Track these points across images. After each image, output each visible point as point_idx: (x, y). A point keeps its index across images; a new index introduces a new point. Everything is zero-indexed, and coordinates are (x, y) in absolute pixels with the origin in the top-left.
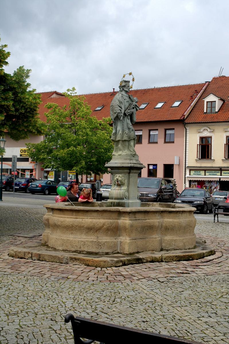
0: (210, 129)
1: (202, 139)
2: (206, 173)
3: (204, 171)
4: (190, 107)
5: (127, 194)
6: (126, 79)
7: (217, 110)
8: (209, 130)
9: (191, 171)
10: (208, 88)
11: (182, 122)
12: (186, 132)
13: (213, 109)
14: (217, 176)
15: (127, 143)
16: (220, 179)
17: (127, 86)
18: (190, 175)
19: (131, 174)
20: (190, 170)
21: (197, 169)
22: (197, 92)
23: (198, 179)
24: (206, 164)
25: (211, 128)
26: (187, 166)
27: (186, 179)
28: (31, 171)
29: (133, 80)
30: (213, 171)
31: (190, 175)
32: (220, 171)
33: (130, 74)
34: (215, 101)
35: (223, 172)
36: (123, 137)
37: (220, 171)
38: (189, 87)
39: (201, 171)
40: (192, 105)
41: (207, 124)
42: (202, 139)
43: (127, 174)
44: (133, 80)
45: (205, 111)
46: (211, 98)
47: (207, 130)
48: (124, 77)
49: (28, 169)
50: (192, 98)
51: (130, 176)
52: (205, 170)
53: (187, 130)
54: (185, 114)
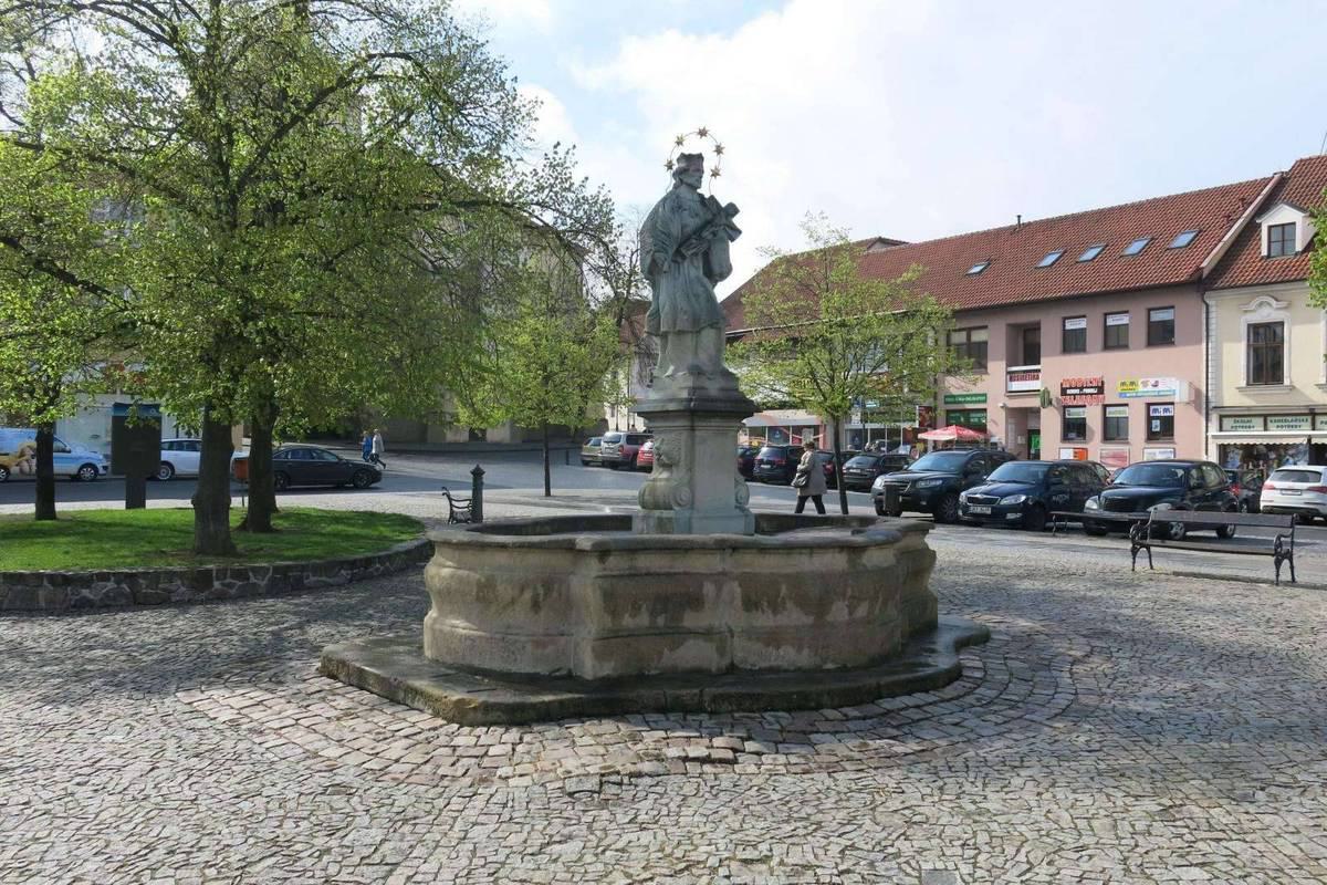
0: (1277, 300)
1: (1255, 329)
2: (1270, 424)
3: (1261, 420)
4: (1221, 244)
5: (685, 494)
6: (691, 148)
7: (1299, 247)
8: (1274, 303)
9: (1225, 421)
10: (1279, 190)
11: (1202, 284)
12: (1207, 313)
13: (1287, 244)
14: (1298, 434)
15: (689, 340)
16: (1309, 440)
17: (692, 168)
18: (1221, 430)
19: (697, 433)
20: (1221, 417)
21: (1242, 416)
22: (1245, 203)
23: (1245, 442)
24: (1268, 397)
25: (1278, 295)
26: (1211, 405)
27: (1210, 440)
28: (816, 429)
29: (719, 150)
30: (1289, 418)
31: (1221, 430)
32: (1309, 418)
33: (703, 133)
34: (1294, 224)
35: (1319, 419)
36: (675, 324)
37: (1309, 418)
38: (1224, 192)
39: (1254, 419)
40: (1225, 239)
41: (1269, 288)
42: (1255, 329)
43: (685, 435)
44: (719, 150)
45: (1264, 252)
46: (1284, 214)
47: (1269, 304)
48: (679, 142)
49: (809, 427)
50: (1230, 220)
51: (697, 440)
52: (1265, 417)
53: (1211, 309)
54: (1203, 265)
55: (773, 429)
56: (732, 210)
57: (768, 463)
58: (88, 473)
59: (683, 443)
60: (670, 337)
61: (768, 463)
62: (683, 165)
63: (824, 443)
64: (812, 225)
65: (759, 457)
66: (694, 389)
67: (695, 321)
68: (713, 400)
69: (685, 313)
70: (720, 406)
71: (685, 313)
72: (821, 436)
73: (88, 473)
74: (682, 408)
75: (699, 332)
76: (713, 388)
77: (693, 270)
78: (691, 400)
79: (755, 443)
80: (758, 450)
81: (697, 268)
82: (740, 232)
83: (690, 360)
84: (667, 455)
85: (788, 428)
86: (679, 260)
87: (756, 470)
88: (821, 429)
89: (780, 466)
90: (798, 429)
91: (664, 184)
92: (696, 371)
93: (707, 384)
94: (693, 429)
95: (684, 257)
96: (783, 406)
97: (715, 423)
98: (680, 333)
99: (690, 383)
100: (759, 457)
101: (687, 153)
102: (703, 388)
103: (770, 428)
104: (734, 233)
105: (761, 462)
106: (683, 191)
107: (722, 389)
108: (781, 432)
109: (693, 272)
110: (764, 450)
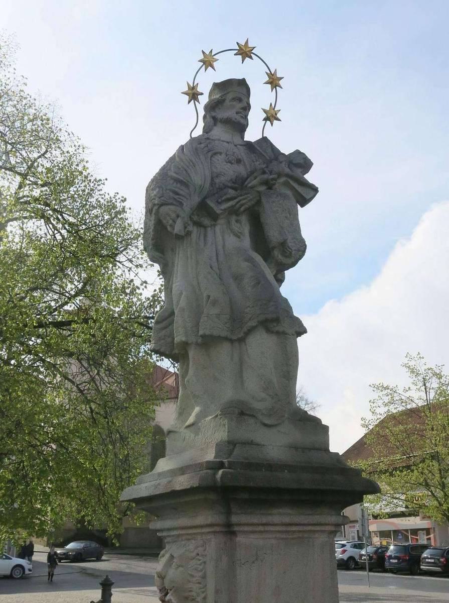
6: (229, 68)
15: (224, 354)
19: (240, 539)
28: (428, 531)
43: (213, 544)
55: (396, 532)
56: (301, 162)
57: (396, 558)
58: (17, 574)
59: (210, 568)
60: (191, 353)
61: (396, 558)
62: (217, 96)
63: (435, 541)
64: (412, 363)
65: (388, 553)
66: (231, 444)
67: (236, 318)
68: (271, 466)
69: (215, 303)
70: (286, 479)
71: (215, 303)
72: (432, 536)
73: (17, 574)
74: (195, 483)
75: (242, 340)
76: (275, 444)
77: (232, 238)
78: (221, 465)
79: (384, 543)
80: (387, 548)
81: (238, 236)
82: (315, 190)
83: (228, 394)
84: (177, 590)
85: (407, 531)
86: (206, 221)
87: (387, 564)
88: (431, 531)
89: (404, 561)
90: (415, 532)
91: (186, 124)
92: (239, 412)
93: (261, 435)
94: (229, 531)
95: (214, 217)
96: (402, 515)
97: (280, 516)
98: (208, 342)
99: (222, 435)
100: (388, 553)
101: (219, 81)
102: (251, 443)
103: (395, 531)
104: (306, 193)
105: (390, 557)
106: (219, 132)
107: (294, 447)
108: (402, 534)
109: (231, 241)
110: (392, 547)
